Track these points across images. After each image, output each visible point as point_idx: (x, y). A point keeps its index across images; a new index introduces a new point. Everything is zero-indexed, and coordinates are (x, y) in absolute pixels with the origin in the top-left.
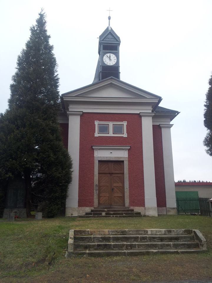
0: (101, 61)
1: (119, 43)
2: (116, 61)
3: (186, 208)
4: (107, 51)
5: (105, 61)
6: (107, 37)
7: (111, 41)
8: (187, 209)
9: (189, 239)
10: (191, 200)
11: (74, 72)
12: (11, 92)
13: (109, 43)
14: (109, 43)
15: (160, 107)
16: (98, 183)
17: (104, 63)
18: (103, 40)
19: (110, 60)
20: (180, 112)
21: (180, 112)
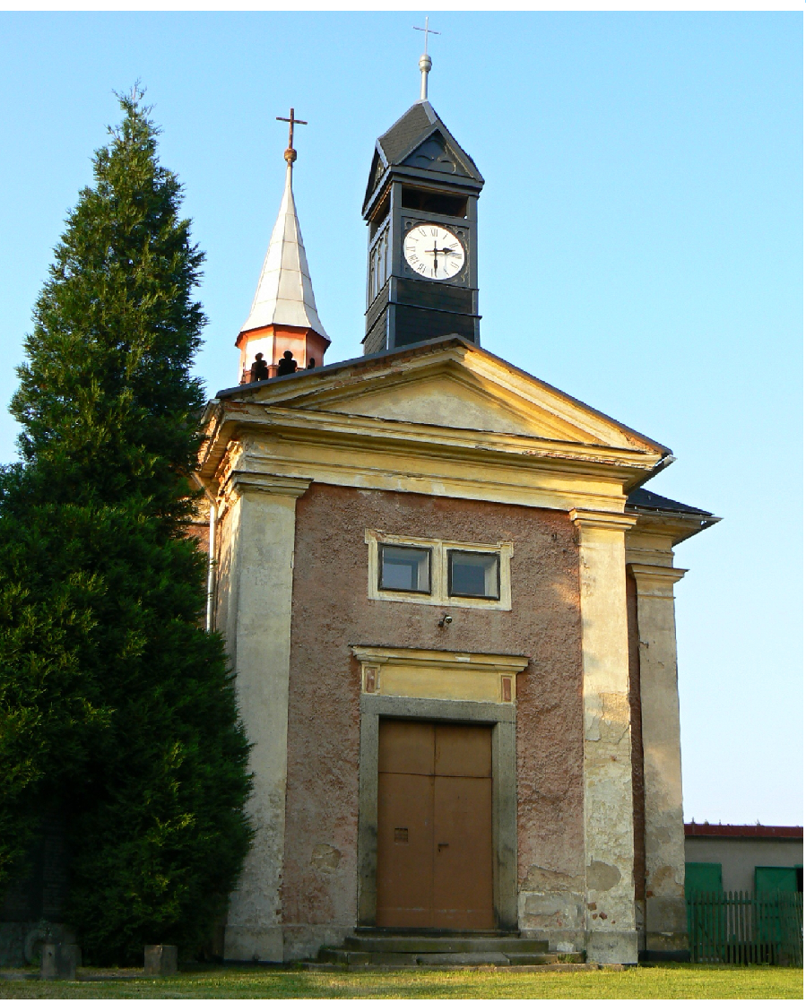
0: (467, 234)
3: (736, 908)
4: (420, 214)
6: (418, 153)
7: (436, 170)
8: (717, 898)
9: (219, 526)
13: (424, 178)
17: (409, 268)
18: (402, 164)
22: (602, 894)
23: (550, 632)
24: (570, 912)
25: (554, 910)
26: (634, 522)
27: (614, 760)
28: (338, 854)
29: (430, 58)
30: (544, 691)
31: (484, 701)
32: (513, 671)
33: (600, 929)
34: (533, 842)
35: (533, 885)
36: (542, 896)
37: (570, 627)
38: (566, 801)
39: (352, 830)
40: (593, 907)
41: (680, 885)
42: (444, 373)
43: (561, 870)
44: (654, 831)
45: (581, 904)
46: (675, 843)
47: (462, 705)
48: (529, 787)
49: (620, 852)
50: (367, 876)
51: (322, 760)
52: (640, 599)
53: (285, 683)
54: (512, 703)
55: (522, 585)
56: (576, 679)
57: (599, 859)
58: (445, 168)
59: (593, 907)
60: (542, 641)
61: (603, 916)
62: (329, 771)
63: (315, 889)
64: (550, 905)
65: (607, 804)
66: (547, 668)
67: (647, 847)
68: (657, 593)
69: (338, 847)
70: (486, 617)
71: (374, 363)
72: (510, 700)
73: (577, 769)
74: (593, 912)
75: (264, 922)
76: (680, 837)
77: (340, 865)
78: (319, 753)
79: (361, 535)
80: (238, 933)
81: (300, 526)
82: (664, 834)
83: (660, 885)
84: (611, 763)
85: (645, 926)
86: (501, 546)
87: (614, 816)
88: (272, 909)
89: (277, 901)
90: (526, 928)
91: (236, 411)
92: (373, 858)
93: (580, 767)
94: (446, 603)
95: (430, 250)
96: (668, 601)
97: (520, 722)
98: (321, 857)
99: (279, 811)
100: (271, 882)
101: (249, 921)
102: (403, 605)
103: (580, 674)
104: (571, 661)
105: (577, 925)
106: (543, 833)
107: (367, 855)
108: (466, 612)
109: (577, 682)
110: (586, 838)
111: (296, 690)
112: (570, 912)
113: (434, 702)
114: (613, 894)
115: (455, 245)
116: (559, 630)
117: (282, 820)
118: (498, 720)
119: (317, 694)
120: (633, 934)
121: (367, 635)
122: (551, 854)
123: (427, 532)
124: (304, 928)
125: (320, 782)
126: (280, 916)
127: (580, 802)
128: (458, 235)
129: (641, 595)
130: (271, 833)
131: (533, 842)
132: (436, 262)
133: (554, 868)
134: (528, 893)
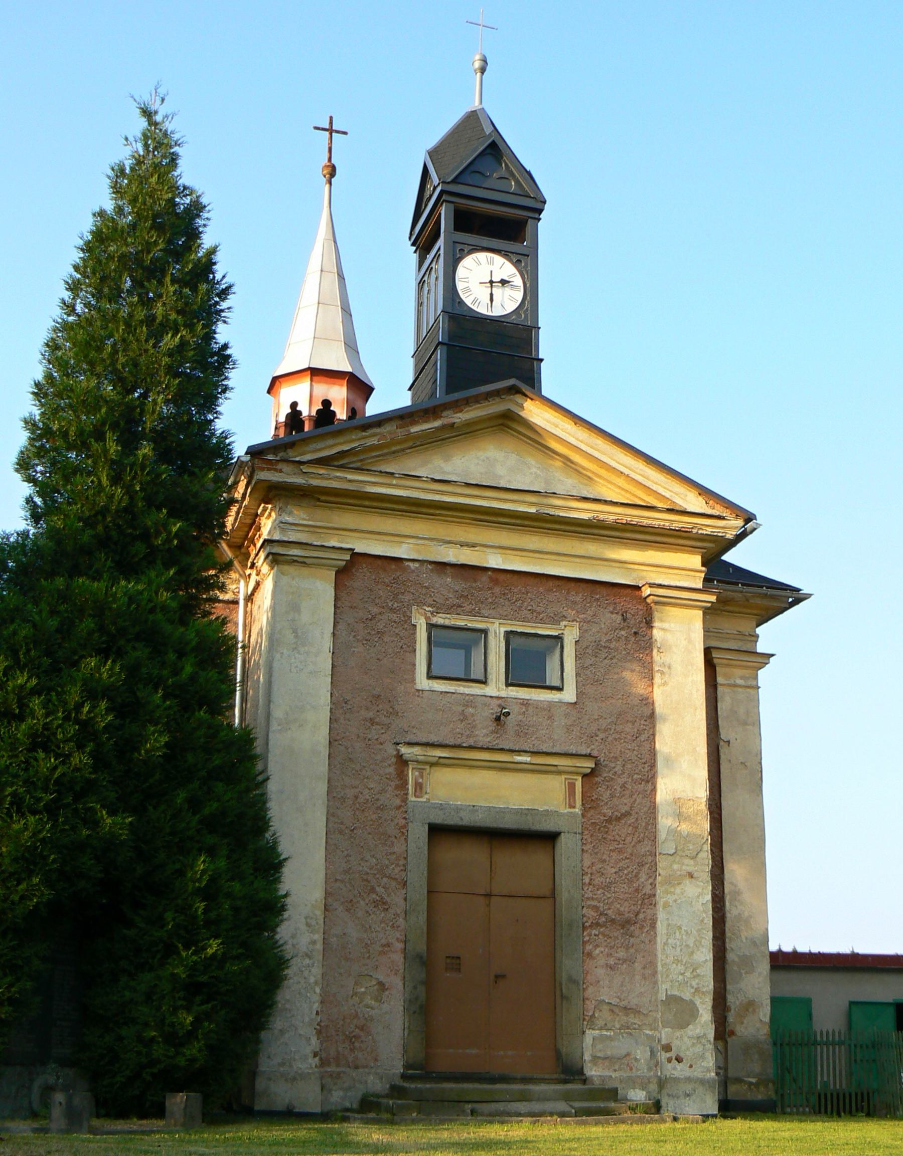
1: (538, 206)
2: (461, 272)
5: (467, 289)
7: (492, 188)
10: (833, 1044)
11: (310, 312)
12: (92, 232)
13: (478, 198)
14: (478, 198)
15: (725, 562)
16: (425, 948)
17: (461, 302)
18: (455, 181)
19: (485, 281)
20: (807, 596)
21: (807, 596)
22: (678, 1034)
24: (641, 1054)
26: (713, 598)
28: (382, 986)
30: (612, 796)
31: (546, 808)
32: (577, 773)
33: (676, 1074)
35: (601, 1023)
37: (642, 722)
40: (667, 1048)
41: (766, 1023)
44: (736, 959)
45: (654, 1044)
46: (760, 974)
48: (596, 908)
49: (698, 984)
50: (415, 1012)
51: (365, 877)
52: (720, 689)
53: (323, 787)
54: (577, 810)
55: (588, 672)
56: (648, 782)
59: (667, 1048)
60: (610, 738)
61: (679, 1060)
62: (373, 890)
64: (620, 1046)
65: (684, 928)
66: (616, 769)
68: (740, 682)
69: (382, 978)
72: (574, 807)
73: (650, 887)
74: (668, 1055)
76: (764, 966)
80: (270, 1079)
82: (747, 962)
84: (687, 881)
86: (565, 626)
87: (691, 942)
88: (308, 1050)
89: (314, 1040)
90: (593, 1073)
91: (269, 469)
93: (653, 885)
94: (503, 694)
95: (485, 281)
97: (586, 832)
98: (363, 990)
100: (307, 1019)
101: (282, 1064)
104: (643, 761)
105: (650, 1069)
106: (612, 961)
107: (415, 988)
108: (525, 703)
109: (650, 786)
110: (660, 968)
112: (641, 1054)
114: (690, 1033)
115: (513, 275)
117: (319, 946)
119: (359, 800)
120: (714, 1080)
122: (622, 985)
125: (362, 902)
126: (317, 1059)
127: (653, 926)
128: (517, 264)
129: (721, 685)
130: (307, 961)
131: (601, 972)
132: (491, 295)
133: (623, 1004)
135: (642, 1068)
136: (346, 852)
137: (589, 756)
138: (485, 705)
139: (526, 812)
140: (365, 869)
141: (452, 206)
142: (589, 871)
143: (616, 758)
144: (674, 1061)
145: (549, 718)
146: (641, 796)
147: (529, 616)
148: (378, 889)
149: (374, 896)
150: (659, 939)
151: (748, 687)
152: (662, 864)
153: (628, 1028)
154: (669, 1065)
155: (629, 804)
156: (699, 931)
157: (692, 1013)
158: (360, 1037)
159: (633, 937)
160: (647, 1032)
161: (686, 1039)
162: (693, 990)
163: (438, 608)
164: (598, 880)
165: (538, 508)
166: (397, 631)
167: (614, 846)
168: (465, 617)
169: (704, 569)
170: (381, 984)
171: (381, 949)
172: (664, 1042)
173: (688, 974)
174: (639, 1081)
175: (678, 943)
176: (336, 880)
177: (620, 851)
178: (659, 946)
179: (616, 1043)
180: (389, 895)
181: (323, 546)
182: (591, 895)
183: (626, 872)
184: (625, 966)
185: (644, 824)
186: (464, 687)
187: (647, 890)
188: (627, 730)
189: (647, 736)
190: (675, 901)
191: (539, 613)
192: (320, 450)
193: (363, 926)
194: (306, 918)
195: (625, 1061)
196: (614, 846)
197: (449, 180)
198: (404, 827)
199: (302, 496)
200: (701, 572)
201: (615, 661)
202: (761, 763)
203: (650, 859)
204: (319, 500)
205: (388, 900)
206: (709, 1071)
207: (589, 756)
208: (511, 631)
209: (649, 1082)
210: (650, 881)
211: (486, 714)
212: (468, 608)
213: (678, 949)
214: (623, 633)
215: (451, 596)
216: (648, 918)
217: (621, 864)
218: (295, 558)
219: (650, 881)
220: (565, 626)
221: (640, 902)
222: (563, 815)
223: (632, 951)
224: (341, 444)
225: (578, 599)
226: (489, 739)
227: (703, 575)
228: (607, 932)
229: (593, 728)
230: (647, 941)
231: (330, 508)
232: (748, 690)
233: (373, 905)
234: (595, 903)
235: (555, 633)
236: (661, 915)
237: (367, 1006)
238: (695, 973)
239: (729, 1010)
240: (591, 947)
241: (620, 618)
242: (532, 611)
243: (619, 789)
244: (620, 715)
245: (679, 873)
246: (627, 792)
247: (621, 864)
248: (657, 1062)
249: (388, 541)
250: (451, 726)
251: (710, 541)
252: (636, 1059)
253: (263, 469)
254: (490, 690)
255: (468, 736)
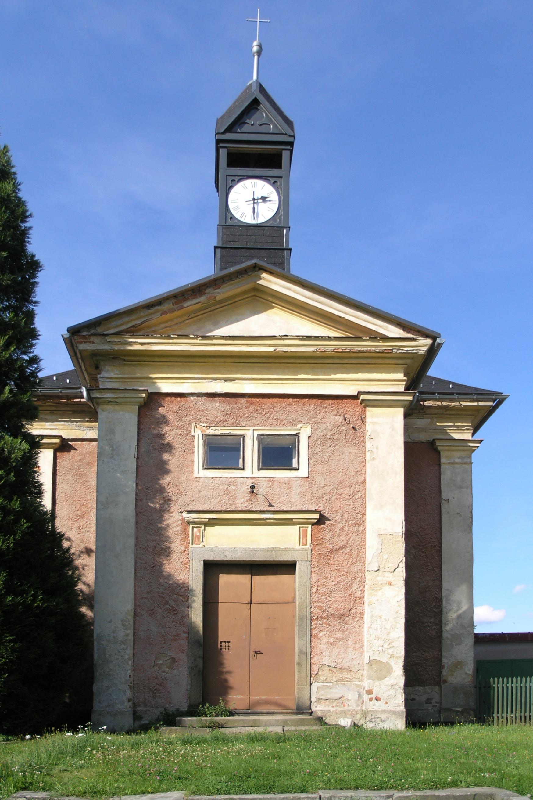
1: (291, 139)
5: (237, 208)
17: (232, 218)
22: (377, 683)
23: (340, 491)
24: (351, 696)
25: (340, 695)
26: (410, 398)
27: (390, 585)
28: (173, 660)
29: (261, 44)
30: (333, 536)
31: (286, 546)
32: (308, 523)
33: (375, 708)
34: (323, 647)
35: (322, 678)
36: (330, 686)
37: (357, 486)
38: (351, 617)
39: (184, 643)
40: (369, 692)
41: (469, 675)
42: (254, 296)
43: (345, 666)
44: (449, 637)
45: (361, 690)
46: (466, 645)
47: (268, 550)
48: (321, 607)
49: (393, 652)
50: (195, 675)
51: (161, 595)
52: (443, 466)
53: (132, 542)
54: (308, 546)
55: (317, 456)
56: (360, 525)
57: (376, 657)
58: (263, 129)
59: (369, 692)
60: (333, 499)
61: (377, 699)
62: (167, 603)
63: (157, 684)
64: (336, 692)
65: (383, 617)
66: (337, 518)
67: (444, 648)
68: (457, 460)
69: (173, 655)
70: (288, 483)
71: (190, 293)
72: (306, 545)
73: (360, 592)
74: (370, 696)
75: (119, 707)
76: (471, 640)
77: (175, 667)
78: (159, 590)
79: (189, 429)
80: (100, 715)
81: (142, 427)
82: (457, 639)
83: (452, 675)
84: (387, 587)
85: (441, 703)
86: (301, 427)
87: (388, 626)
88: (125, 698)
89: (128, 692)
90: (318, 708)
91: (85, 342)
92: (200, 662)
93: (363, 591)
94: (255, 475)
95: (252, 200)
96: (466, 466)
97: (314, 560)
98: (161, 662)
99: (129, 632)
100: (123, 680)
101: (109, 706)
102: (221, 479)
103: (364, 521)
104: (357, 512)
105: (358, 705)
106: (331, 640)
107: (195, 660)
108: (271, 480)
109: (361, 528)
110: (365, 643)
111: (141, 546)
112: (351, 696)
113: (245, 549)
114: (386, 683)
115: (272, 192)
116: (347, 489)
117: (131, 637)
118: (296, 559)
119: (157, 549)
120: (402, 711)
121: (194, 503)
122: (338, 655)
123: (241, 423)
124: (149, 710)
125: (159, 610)
126: (130, 703)
127: (362, 617)
128: (274, 184)
129: (444, 464)
130: (123, 646)
131: (323, 647)
132: (254, 208)
133: (339, 666)
134: (320, 684)
135: (352, 705)
136: (149, 581)
137: (315, 512)
138: (243, 483)
139: (271, 549)
140: (162, 590)
141: (225, 150)
142: (316, 584)
143: (336, 511)
144: (374, 700)
145: (288, 488)
146: (354, 534)
147: (275, 423)
148: (170, 602)
149: (168, 606)
150: (365, 625)
151: (464, 463)
152: (369, 576)
153: (342, 681)
154: (371, 702)
155: (345, 541)
156: (395, 618)
157: (389, 670)
158: (159, 690)
159: (347, 624)
160: (356, 683)
161: (383, 687)
162: (389, 656)
163: (210, 423)
164: (322, 590)
165: (275, 348)
166: (182, 441)
167: (335, 567)
168: (229, 428)
169: (405, 378)
170: (173, 658)
171: (173, 638)
172: (366, 689)
173: (386, 646)
174: (349, 713)
175: (379, 627)
176: (143, 598)
177: (339, 571)
178: (365, 629)
179: (333, 690)
180: (178, 605)
181: (126, 389)
182: (317, 599)
183: (342, 584)
184: (341, 643)
185: (356, 553)
186: (229, 473)
187: (358, 594)
188: (346, 492)
189: (360, 495)
190: (378, 600)
191: (282, 421)
192: (119, 326)
193: (160, 624)
194: (122, 621)
195: (341, 701)
196: (335, 567)
197: (222, 131)
198: (187, 563)
199: (113, 358)
200: (402, 381)
201: (337, 447)
202: (472, 512)
203: (360, 575)
204: (124, 360)
205: (177, 608)
206: (399, 706)
207: (315, 512)
208: (262, 435)
209: (357, 714)
210: (361, 588)
211: (244, 489)
212: (231, 422)
213: (379, 631)
214: (344, 428)
215: (219, 414)
216: (359, 612)
217: (339, 579)
218: (109, 399)
219: (361, 588)
220: (301, 427)
221: (352, 603)
222: (297, 550)
223: (346, 633)
224: (134, 320)
225: (311, 408)
226: (245, 505)
227: (404, 383)
228: (328, 622)
229: (320, 493)
230: (357, 626)
231: (134, 365)
232: (464, 465)
233: (167, 611)
234: (320, 604)
235: (294, 433)
236: (367, 609)
237: (164, 672)
238: (391, 646)
239: (444, 667)
240: (317, 632)
241: (341, 418)
242: (277, 420)
243: (338, 531)
244: (341, 483)
245: (381, 582)
246: (345, 533)
247: (339, 579)
248: (363, 701)
249: (171, 383)
250: (219, 498)
251: (409, 358)
252: (348, 700)
253: (81, 343)
254: (247, 473)
255: (231, 504)
